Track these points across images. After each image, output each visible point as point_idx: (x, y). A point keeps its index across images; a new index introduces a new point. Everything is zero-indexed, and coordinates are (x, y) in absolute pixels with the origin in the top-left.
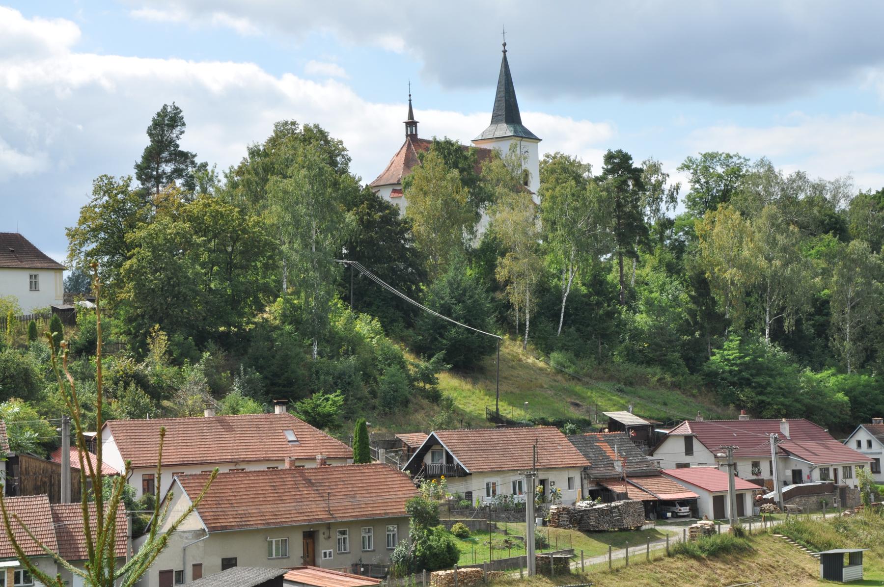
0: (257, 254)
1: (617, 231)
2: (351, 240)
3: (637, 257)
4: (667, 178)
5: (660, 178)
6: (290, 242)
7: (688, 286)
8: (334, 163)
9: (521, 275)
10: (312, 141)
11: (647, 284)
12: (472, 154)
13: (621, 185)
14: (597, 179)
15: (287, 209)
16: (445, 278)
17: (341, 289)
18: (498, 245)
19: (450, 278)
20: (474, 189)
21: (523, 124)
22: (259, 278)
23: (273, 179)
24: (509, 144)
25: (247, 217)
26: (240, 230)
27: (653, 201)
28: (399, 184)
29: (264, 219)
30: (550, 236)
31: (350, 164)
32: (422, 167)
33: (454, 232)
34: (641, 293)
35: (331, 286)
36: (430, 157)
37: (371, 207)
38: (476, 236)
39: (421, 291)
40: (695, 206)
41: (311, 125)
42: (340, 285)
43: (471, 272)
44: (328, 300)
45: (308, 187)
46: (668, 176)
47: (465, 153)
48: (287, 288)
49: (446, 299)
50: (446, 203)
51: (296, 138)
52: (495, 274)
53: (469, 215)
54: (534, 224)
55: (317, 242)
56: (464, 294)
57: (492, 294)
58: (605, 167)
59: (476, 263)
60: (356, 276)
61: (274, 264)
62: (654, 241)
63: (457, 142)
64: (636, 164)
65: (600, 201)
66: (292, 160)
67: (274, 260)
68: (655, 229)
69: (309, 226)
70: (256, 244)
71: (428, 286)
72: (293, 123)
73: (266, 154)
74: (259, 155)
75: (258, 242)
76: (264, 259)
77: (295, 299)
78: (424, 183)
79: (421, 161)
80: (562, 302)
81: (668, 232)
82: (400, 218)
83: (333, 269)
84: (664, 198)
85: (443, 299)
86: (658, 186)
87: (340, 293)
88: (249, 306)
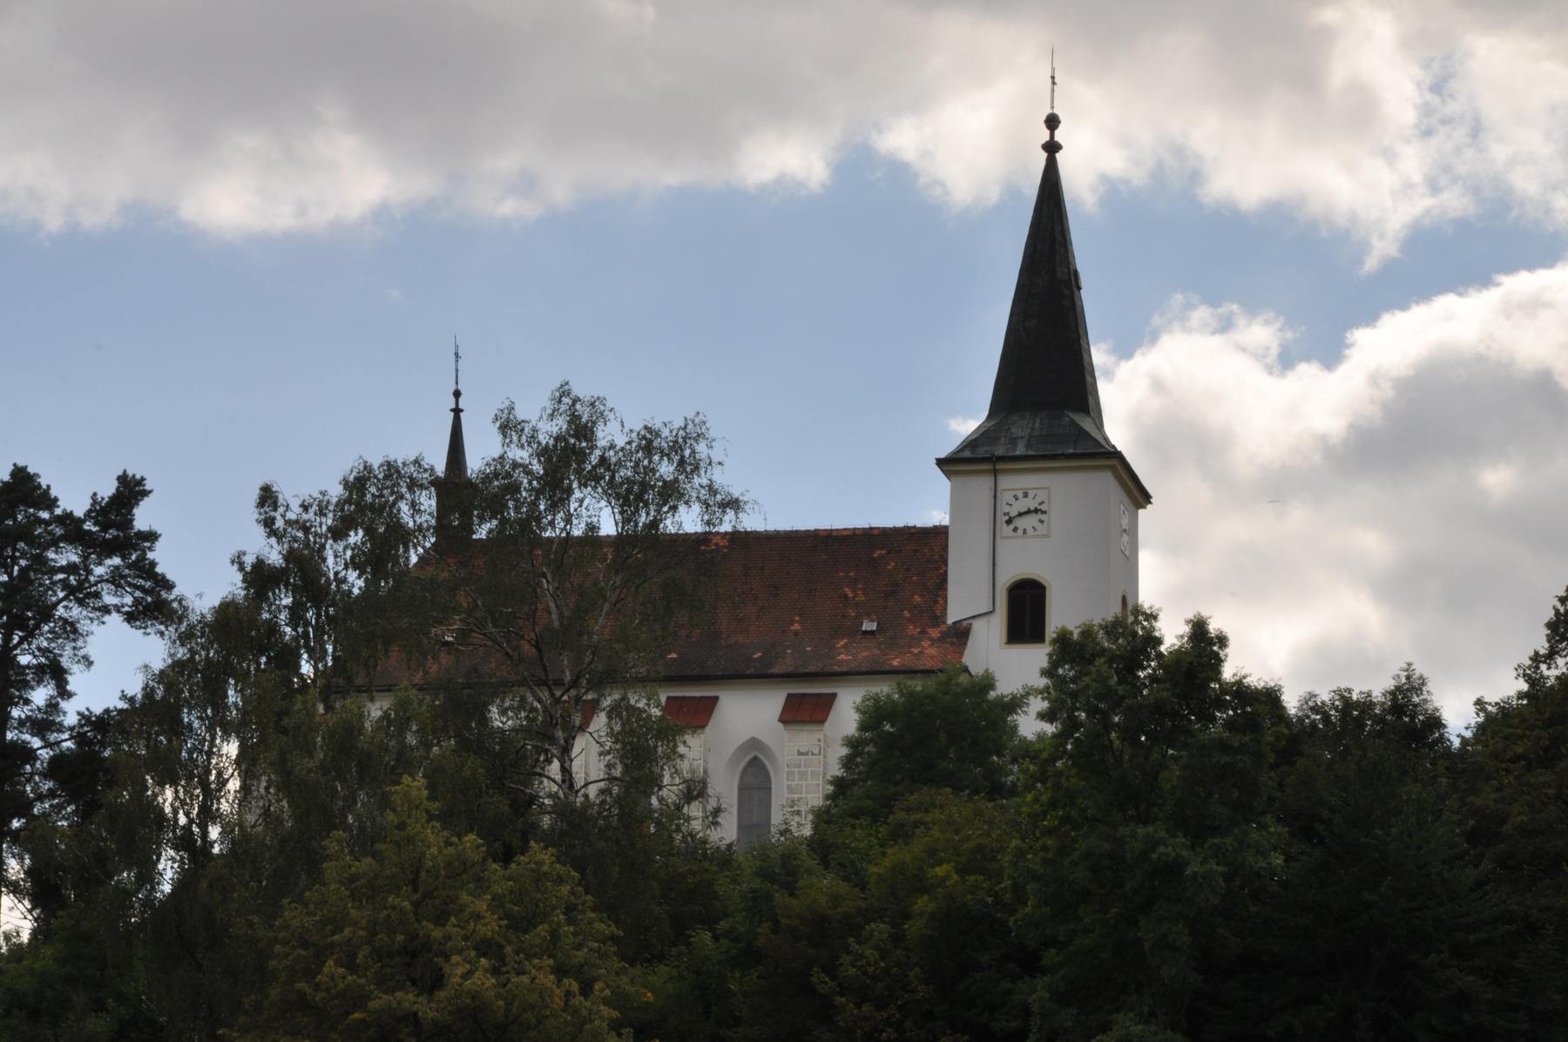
82: (1075, 636)
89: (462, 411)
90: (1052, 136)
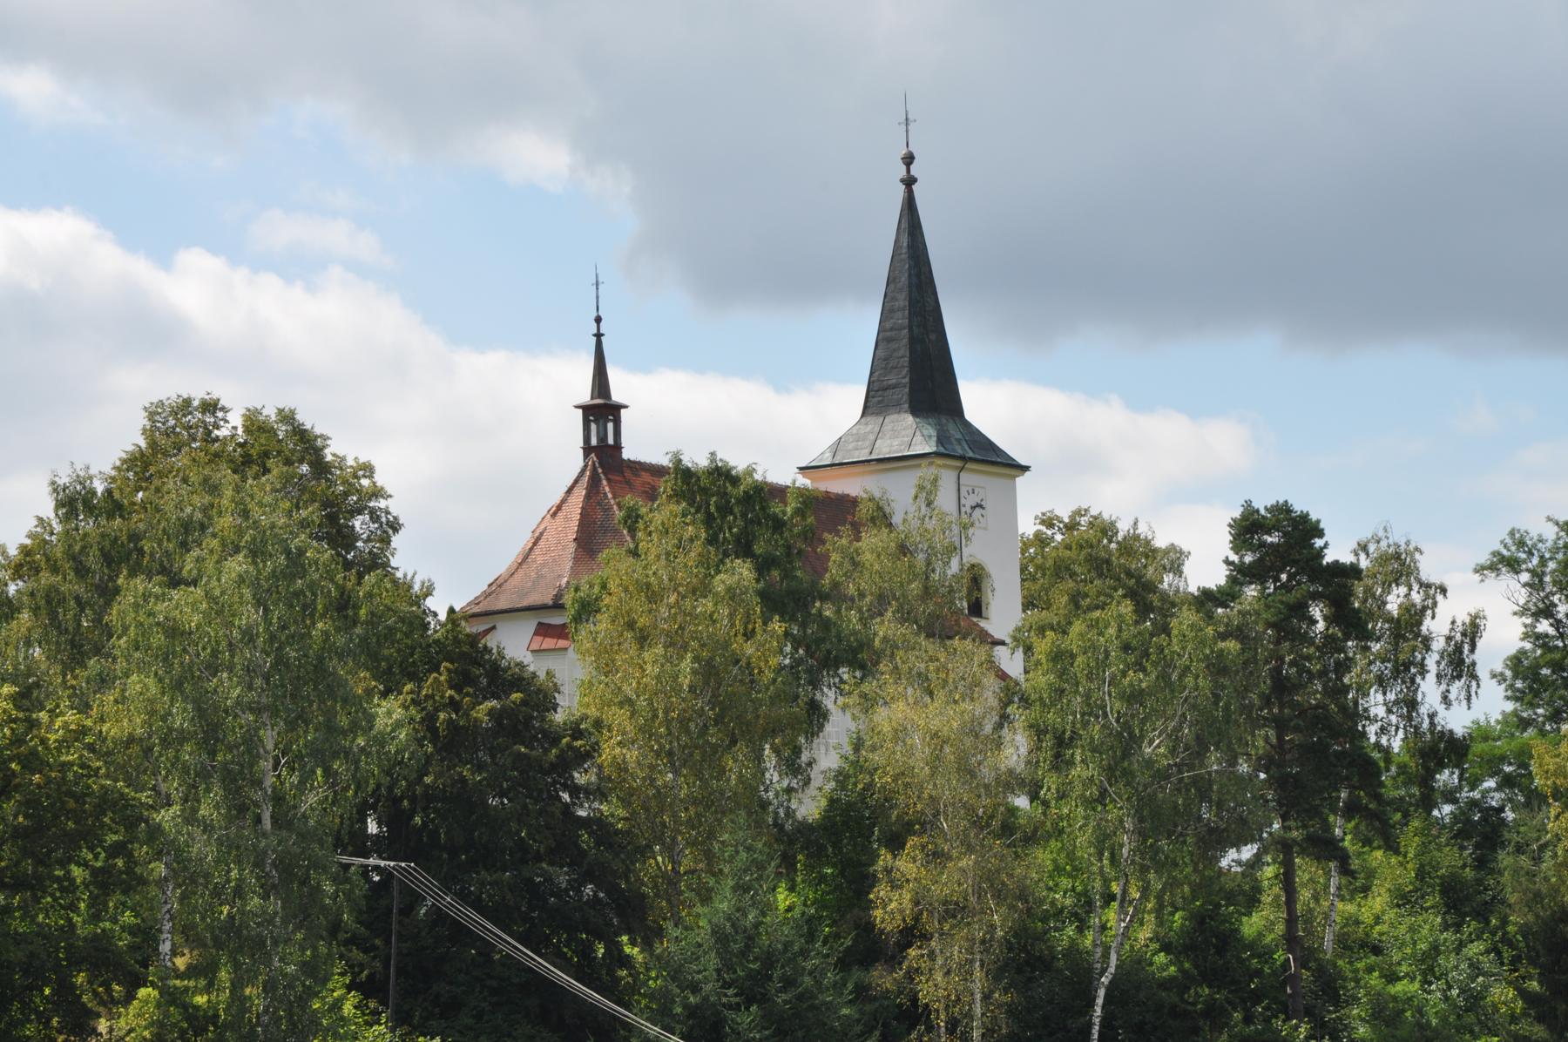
0: (72, 841)
1: (1274, 770)
2: (390, 788)
3: (1343, 859)
4: (1439, 598)
5: (1417, 597)
6: (186, 800)
7: (1515, 961)
8: (341, 538)
9: (954, 911)
10: (270, 463)
11: (1377, 950)
12: (797, 512)
13: (1287, 619)
14: (1207, 599)
15: (178, 686)
16: (704, 920)
17: (357, 955)
18: (881, 811)
19: (719, 919)
20: (803, 626)
21: (969, 416)
22: (77, 919)
23: (134, 587)
24: (915, 481)
25: (43, 716)
26: (16, 758)
27: (1396, 673)
28: (557, 606)
29: (102, 720)
30: (1051, 783)
31: (396, 541)
32: (635, 553)
33: (735, 766)
34: (1357, 981)
35: (323, 948)
36: (658, 518)
37: (461, 681)
38: (807, 782)
39: (626, 961)
40: (1536, 694)
41: (270, 413)
42: (353, 941)
43: (793, 899)
44: (311, 993)
45: (250, 615)
46: (1444, 591)
47: (776, 508)
48: (174, 953)
49: (708, 987)
50: (708, 672)
51: (217, 455)
52: (870, 905)
53: (783, 710)
54: (999, 744)
55: (278, 799)
56: (763, 977)
57: (857, 974)
58: (1234, 558)
59: (809, 868)
60: (408, 909)
61: (129, 871)
62: (1399, 805)
63: (750, 471)
64: (1337, 550)
65: (1218, 667)
66: (203, 527)
67: (129, 856)
68: (1402, 768)
69: (251, 741)
70: (71, 804)
71: (647, 946)
72: (211, 406)
73: (113, 506)
74: (90, 509)
75: (80, 798)
76: (96, 857)
77: (197, 991)
78: (639, 605)
79: (632, 531)
80: (1091, 1003)
81: (1446, 777)
82: (559, 717)
83: (328, 887)
84: (1431, 662)
85: (695, 989)
86: (1409, 624)
87: (353, 968)
88: (39, 1015)
89: (603, 335)
90: (908, 171)
